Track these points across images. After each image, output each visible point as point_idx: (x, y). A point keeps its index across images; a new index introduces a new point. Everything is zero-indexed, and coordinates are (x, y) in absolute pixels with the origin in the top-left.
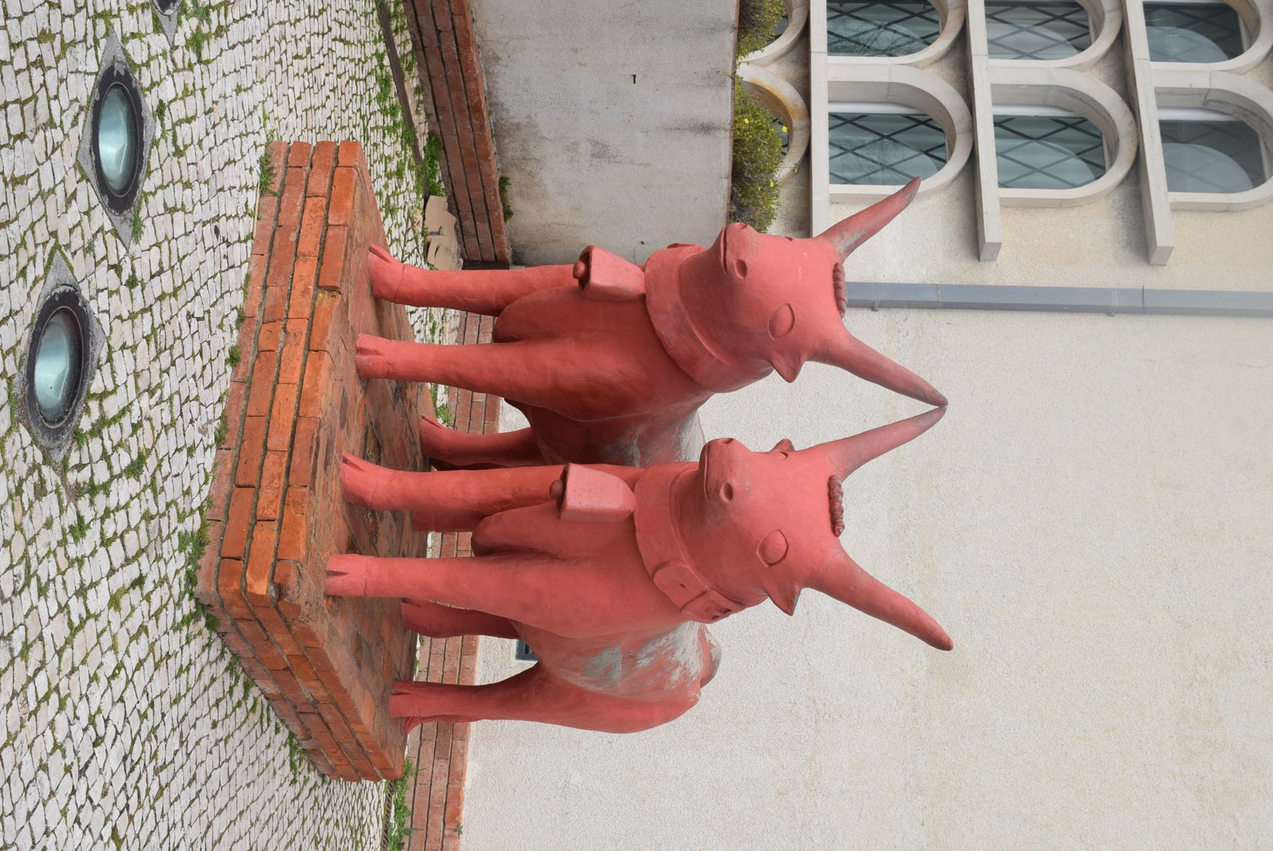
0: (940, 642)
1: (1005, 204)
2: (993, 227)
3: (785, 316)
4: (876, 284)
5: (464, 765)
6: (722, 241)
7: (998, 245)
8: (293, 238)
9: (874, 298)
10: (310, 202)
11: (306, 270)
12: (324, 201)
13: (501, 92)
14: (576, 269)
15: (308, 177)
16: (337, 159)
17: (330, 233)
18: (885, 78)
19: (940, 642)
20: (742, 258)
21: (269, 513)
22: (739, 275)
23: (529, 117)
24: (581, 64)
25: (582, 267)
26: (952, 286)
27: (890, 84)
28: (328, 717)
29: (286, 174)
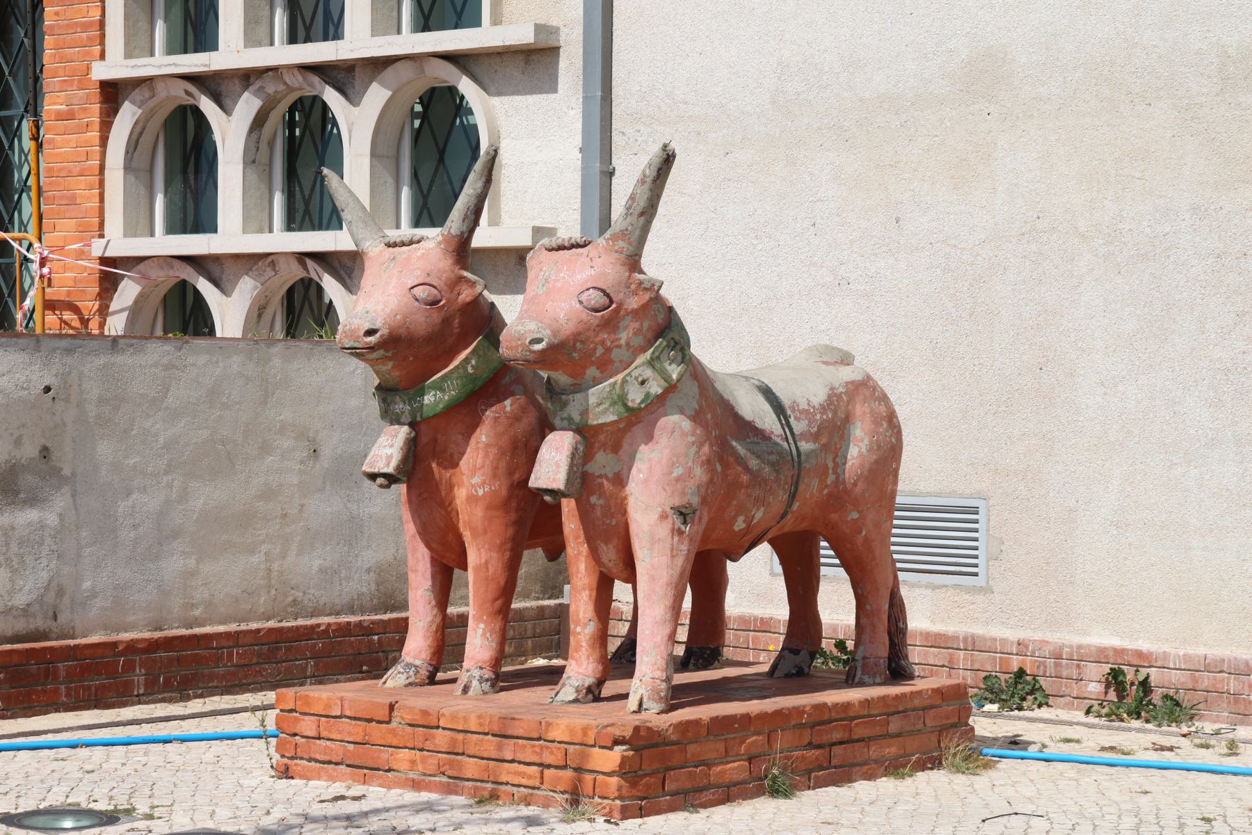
0: (668, 160)
1: (496, 21)
2: (518, 33)
3: (421, 292)
4: (583, 169)
5: (1089, 646)
6: (357, 353)
7: (539, 28)
8: (351, 747)
9: (597, 170)
10: (324, 734)
11: (376, 731)
12: (323, 719)
13: (337, 601)
14: (381, 486)
15: (303, 737)
16: (291, 711)
17: (348, 713)
18: (366, 161)
19: (668, 160)
20: (362, 332)
21: (560, 755)
22: (378, 335)
23: (369, 571)
24: (301, 511)
25: (380, 480)
26: (584, 85)
27: (373, 155)
28: (837, 736)
29: (302, 758)
